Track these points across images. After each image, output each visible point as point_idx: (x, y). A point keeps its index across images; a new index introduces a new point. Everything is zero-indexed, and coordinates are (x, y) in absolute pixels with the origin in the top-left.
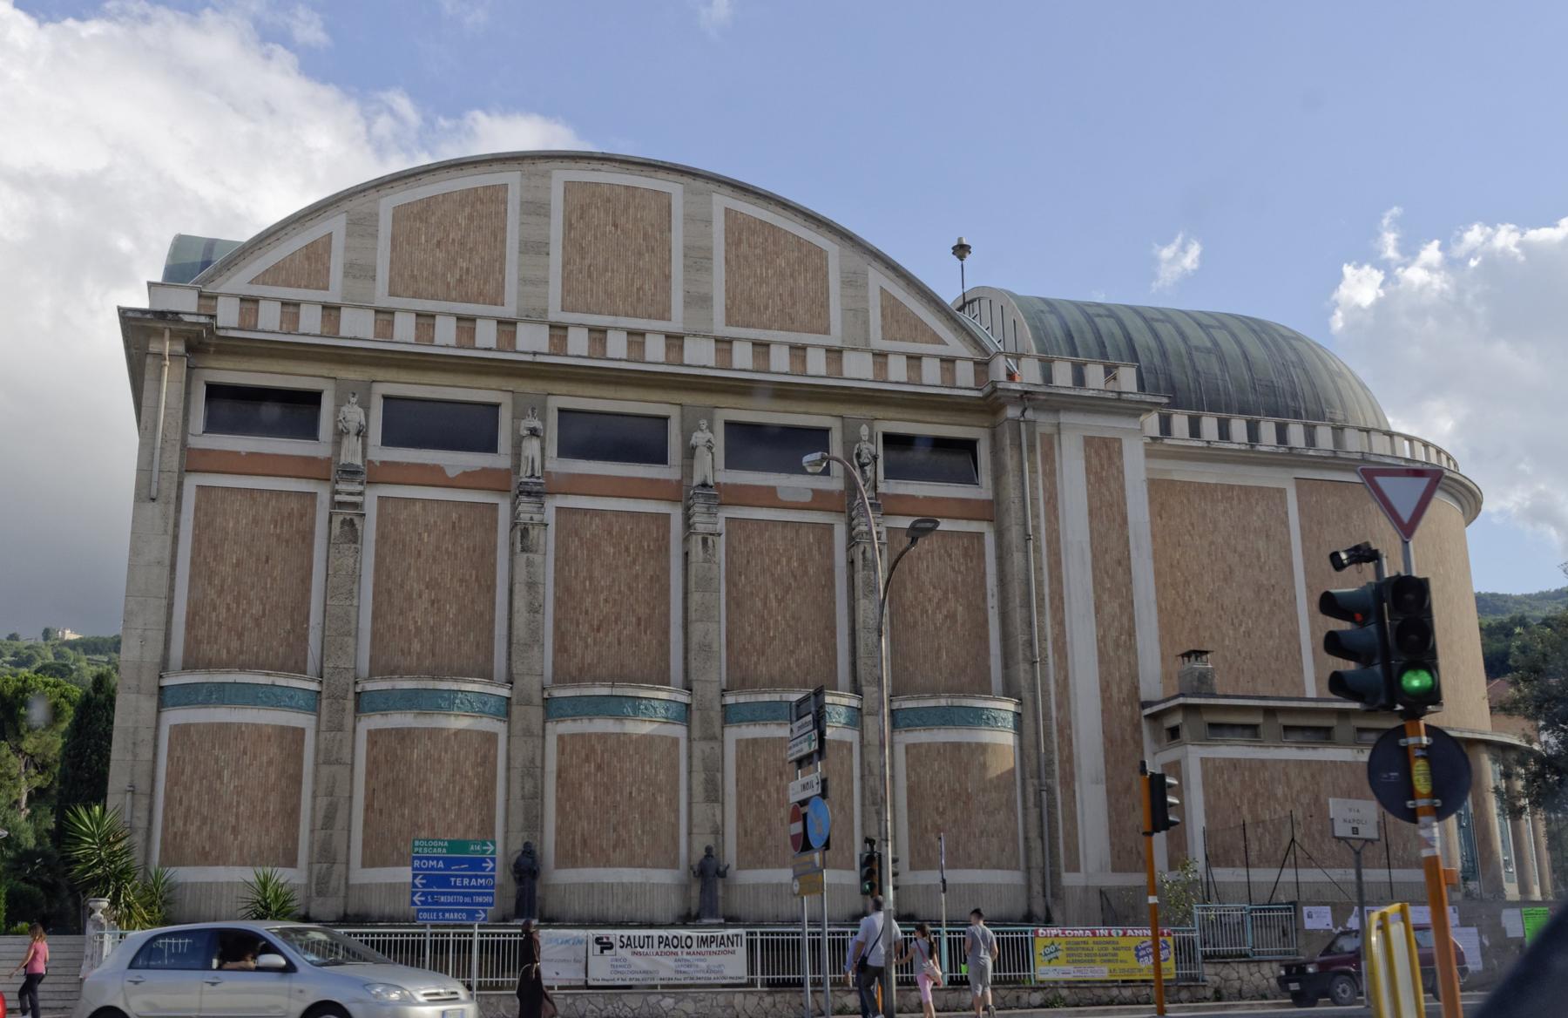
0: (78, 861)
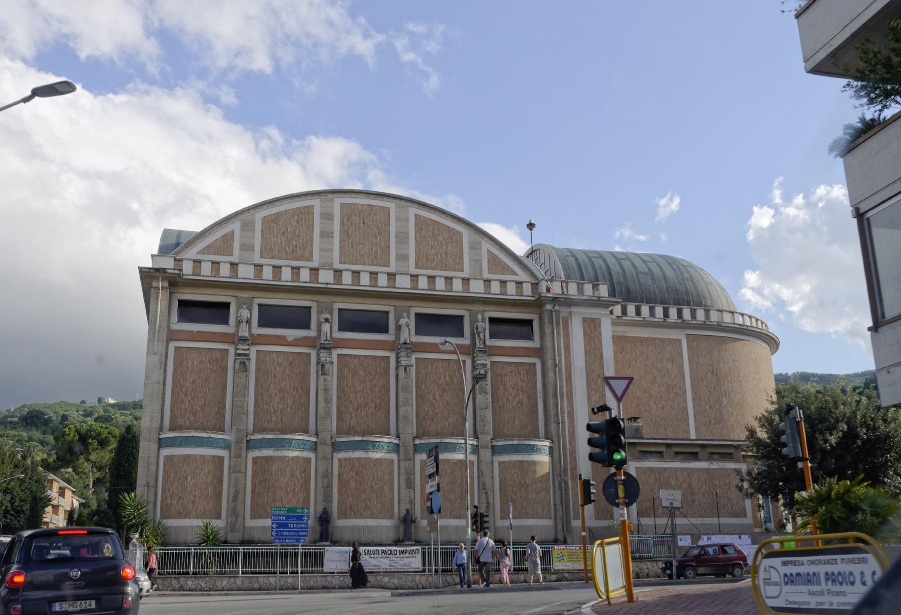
0: (125, 517)
